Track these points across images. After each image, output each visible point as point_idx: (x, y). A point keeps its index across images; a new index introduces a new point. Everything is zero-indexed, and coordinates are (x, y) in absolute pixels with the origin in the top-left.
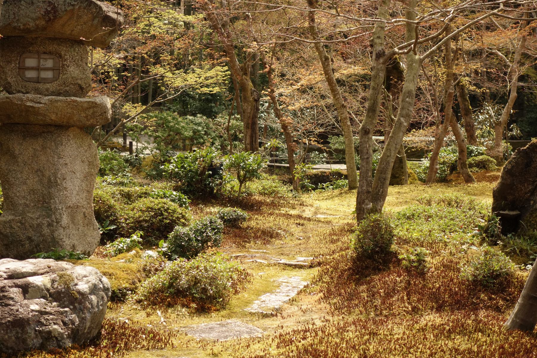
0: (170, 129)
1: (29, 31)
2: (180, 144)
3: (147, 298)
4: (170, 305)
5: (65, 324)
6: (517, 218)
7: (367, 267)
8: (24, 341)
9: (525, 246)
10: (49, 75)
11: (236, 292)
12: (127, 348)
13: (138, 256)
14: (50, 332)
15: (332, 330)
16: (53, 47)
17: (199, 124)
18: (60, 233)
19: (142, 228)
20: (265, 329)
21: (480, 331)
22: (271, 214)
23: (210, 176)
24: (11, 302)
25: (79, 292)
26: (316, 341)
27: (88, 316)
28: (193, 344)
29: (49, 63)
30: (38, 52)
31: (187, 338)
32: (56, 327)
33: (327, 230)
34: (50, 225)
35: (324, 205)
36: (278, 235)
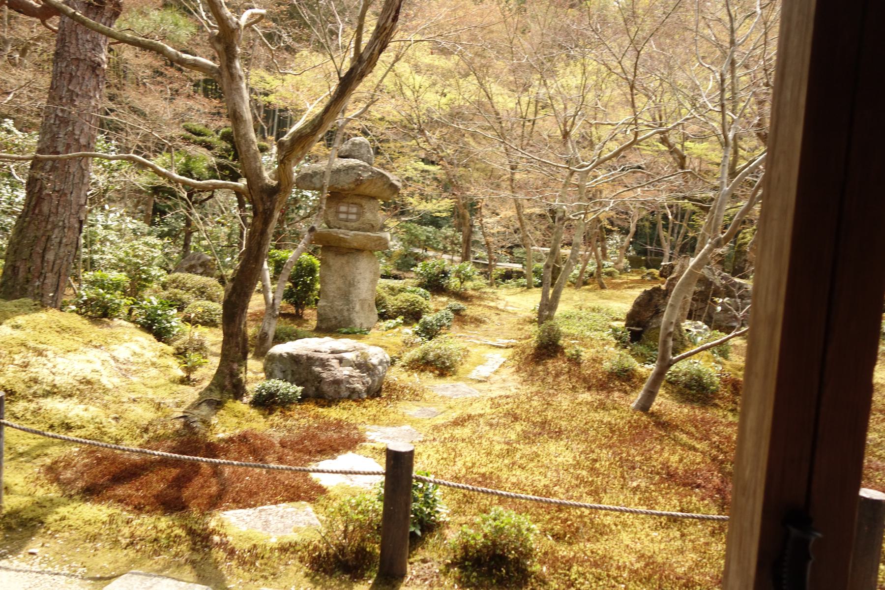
0: (412, 234)
1: (344, 190)
4: (422, 371)
5: (363, 384)
6: (640, 333)
7: (543, 354)
8: (339, 393)
9: (644, 351)
10: (353, 217)
11: (462, 364)
12: (398, 399)
13: (399, 332)
14: (354, 389)
15: (523, 398)
16: (357, 200)
17: (430, 232)
18: (354, 316)
19: (402, 314)
20: (480, 391)
22: (480, 305)
25: (372, 365)
27: (377, 379)
28: (437, 399)
29: (354, 210)
30: (348, 203)
33: (514, 320)
34: (348, 310)
35: (511, 299)
36: (484, 322)
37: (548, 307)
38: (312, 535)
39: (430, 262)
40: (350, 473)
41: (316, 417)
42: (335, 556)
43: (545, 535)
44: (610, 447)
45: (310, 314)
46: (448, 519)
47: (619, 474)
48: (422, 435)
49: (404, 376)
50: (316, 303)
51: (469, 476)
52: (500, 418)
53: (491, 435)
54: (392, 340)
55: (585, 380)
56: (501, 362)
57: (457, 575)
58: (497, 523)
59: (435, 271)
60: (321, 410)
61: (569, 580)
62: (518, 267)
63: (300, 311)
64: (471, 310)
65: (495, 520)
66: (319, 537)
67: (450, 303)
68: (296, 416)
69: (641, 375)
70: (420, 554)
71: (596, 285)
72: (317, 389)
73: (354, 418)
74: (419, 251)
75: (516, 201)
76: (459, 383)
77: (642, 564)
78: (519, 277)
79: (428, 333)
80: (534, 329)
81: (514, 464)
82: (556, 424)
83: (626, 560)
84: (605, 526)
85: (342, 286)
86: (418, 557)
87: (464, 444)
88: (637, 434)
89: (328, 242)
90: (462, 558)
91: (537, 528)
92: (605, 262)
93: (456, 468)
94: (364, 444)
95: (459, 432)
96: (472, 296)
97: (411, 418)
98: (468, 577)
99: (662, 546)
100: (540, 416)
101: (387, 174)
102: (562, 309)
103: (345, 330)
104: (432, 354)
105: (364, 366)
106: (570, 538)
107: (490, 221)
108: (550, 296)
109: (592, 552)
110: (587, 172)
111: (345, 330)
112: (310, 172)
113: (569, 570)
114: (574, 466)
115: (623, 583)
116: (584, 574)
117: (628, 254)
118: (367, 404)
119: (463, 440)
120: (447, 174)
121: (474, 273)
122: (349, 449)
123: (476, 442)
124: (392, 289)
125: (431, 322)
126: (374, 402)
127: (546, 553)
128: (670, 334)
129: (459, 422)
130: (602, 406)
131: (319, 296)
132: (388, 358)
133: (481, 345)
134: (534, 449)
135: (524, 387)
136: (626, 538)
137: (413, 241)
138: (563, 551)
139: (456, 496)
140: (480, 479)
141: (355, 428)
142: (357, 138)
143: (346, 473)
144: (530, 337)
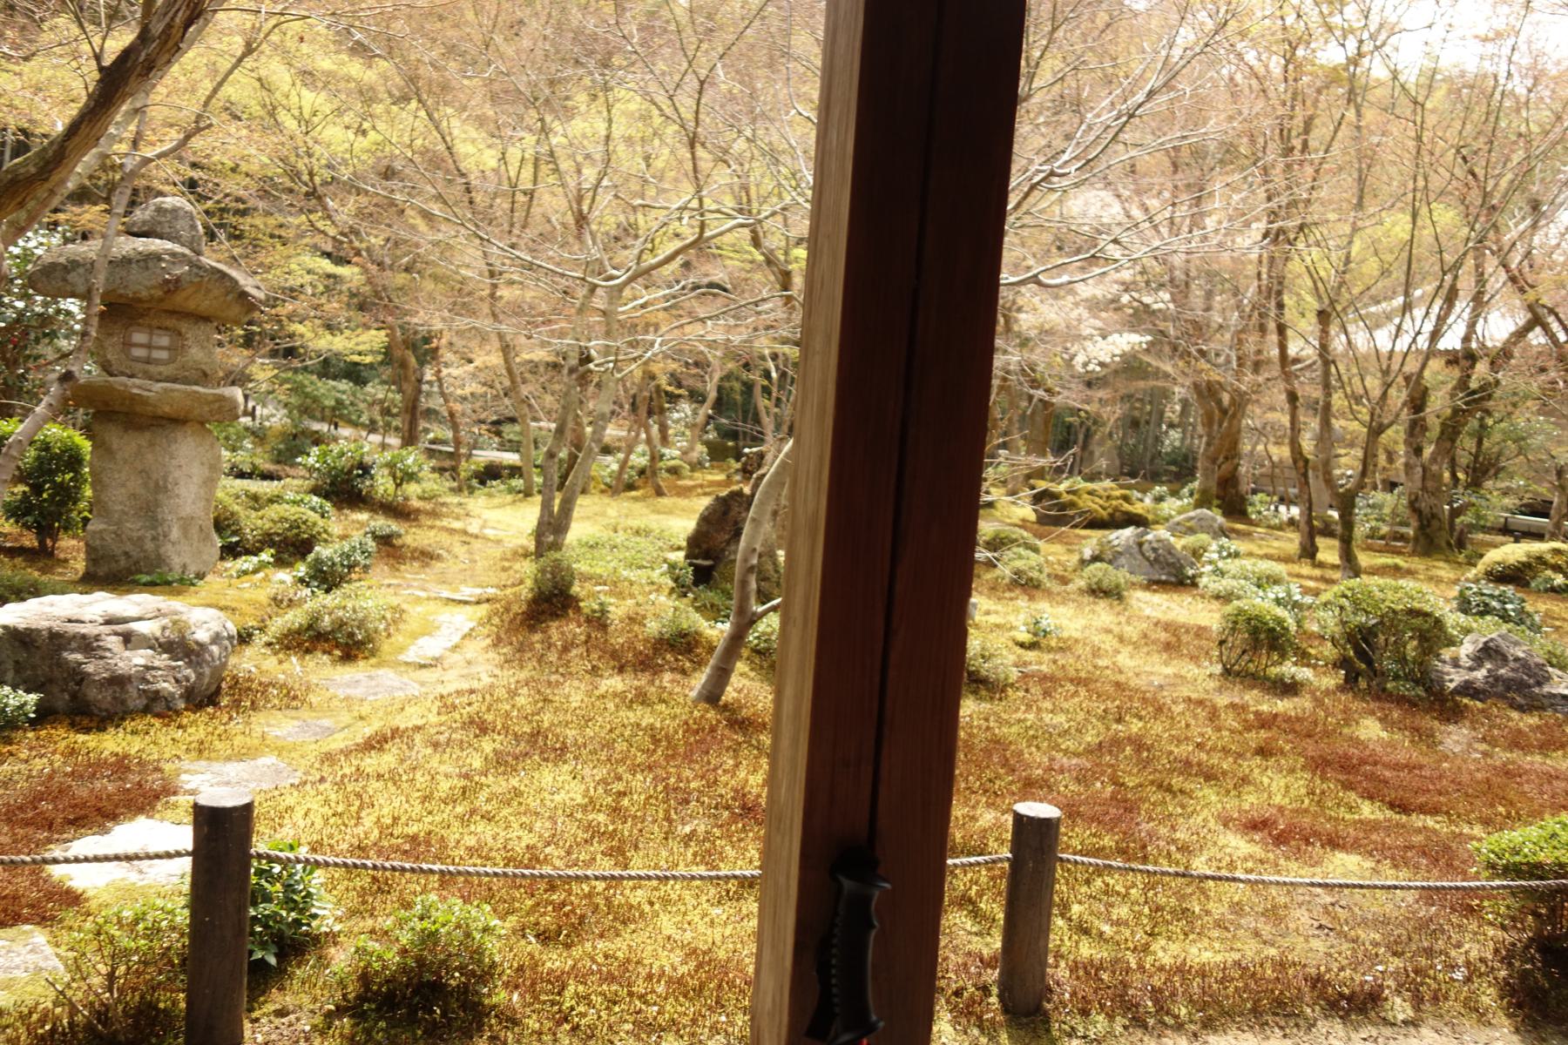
0: (307, 395)
1: (140, 300)
2: (318, 414)
3: (279, 641)
4: (308, 651)
5: (177, 681)
6: (710, 569)
7: (543, 612)
8: (123, 702)
9: (717, 601)
10: (164, 355)
11: (389, 635)
12: (254, 707)
13: (266, 579)
14: (157, 692)
15: (501, 693)
16: (170, 322)
17: (344, 392)
19: (272, 544)
20: (422, 684)
21: (664, 701)
22: (432, 527)
23: (359, 476)
24: (108, 654)
25: (197, 643)
26: (484, 709)
27: (207, 671)
28: (335, 703)
29: (165, 341)
30: (150, 326)
31: (328, 695)
32: (165, 685)
33: (497, 552)
34: (154, 539)
35: (493, 515)
36: (439, 558)
37: (552, 528)
38: (40, 990)
39: (335, 448)
40: (137, 857)
41: (72, 752)
42: (89, 1027)
43: (524, 936)
44: (650, 768)
45: (71, 547)
46: (337, 928)
47: (661, 815)
48: (299, 774)
49: (270, 663)
50: (85, 525)
51: (385, 843)
52: (454, 730)
53: (434, 763)
54: (247, 596)
55: (614, 655)
56: (466, 630)
57: (346, 1031)
58: (425, 924)
59: (343, 462)
60: (81, 738)
61: (560, 1011)
62: (511, 458)
63: (49, 542)
64: (413, 537)
65: (422, 919)
66: (52, 995)
67: (372, 523)
68: (24, 754)
69: (709, 642)
70: (276, 999)
71: (650, 490)
72: (74, 696)
73: (155, 749)
74: (323, 427)
75: (501, 336)
76: (381, 672)
77: (692, 964)
78: (512, 476)
79: (324, 580)
80: (528, 568)
81: (473, 812)
82: (557, 736)
83: (665, 962)
84: (631, 907)
85: (141, 491)
86: (270, 1007)
87: (380, 785)
88: (698, 741)
89: (106, 404)
90: (358, 997)
91: (504, 926)
92: (666, 451)
93: (360, 830)
94: (173, 799)
95: (371, 763)
96: (418, 511)
97: (279, 743)
98: (368, 1032)
99: (728, 932)
100: (530, 722)
101: (234, 273)
102: (579, 531)
103: (145, 578)
104: (327, 618)
105: (179, 647)
106: (568, 936)
107: (455, 371)
108: (556, 509)
109: (606, 957)
110: (621, 288)
111: (145, 578)
112: (62, 260)
113: (559, 994)
114: (584, 808)
115: (655, 1004)
116: (586, 997)
117: (705, 437)
118: (185, 721)
119: (379, 776)
120: (369, 281)
121: (421, 469)
122: (141, 810)
123: (405, 778)
124: (255, 498)
125: (331, 559)
126: (202, 717)
127: (521, 969)
128: (751, 569)
129: (375, 744)
130: (642, 698)
131: (90, 512)
132: (232, 629)
133: (429, 599)
134: (514, 782)
135: (506, 673)
136: (667, 924)
137: (308, 407)
138: (554, 960)
139: (358, 883)
140: (407, 847)
141: (157, 769)
142: (168, 199)
143: (129, 858)
144: (521, 582)
